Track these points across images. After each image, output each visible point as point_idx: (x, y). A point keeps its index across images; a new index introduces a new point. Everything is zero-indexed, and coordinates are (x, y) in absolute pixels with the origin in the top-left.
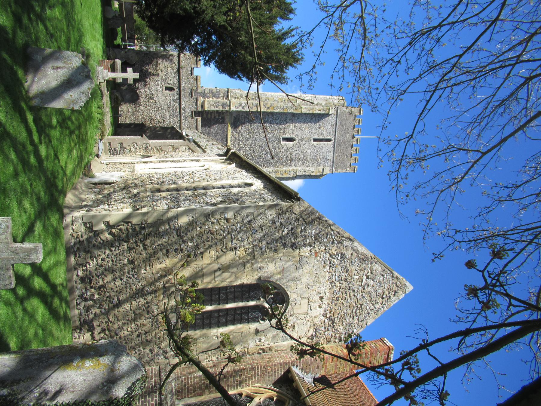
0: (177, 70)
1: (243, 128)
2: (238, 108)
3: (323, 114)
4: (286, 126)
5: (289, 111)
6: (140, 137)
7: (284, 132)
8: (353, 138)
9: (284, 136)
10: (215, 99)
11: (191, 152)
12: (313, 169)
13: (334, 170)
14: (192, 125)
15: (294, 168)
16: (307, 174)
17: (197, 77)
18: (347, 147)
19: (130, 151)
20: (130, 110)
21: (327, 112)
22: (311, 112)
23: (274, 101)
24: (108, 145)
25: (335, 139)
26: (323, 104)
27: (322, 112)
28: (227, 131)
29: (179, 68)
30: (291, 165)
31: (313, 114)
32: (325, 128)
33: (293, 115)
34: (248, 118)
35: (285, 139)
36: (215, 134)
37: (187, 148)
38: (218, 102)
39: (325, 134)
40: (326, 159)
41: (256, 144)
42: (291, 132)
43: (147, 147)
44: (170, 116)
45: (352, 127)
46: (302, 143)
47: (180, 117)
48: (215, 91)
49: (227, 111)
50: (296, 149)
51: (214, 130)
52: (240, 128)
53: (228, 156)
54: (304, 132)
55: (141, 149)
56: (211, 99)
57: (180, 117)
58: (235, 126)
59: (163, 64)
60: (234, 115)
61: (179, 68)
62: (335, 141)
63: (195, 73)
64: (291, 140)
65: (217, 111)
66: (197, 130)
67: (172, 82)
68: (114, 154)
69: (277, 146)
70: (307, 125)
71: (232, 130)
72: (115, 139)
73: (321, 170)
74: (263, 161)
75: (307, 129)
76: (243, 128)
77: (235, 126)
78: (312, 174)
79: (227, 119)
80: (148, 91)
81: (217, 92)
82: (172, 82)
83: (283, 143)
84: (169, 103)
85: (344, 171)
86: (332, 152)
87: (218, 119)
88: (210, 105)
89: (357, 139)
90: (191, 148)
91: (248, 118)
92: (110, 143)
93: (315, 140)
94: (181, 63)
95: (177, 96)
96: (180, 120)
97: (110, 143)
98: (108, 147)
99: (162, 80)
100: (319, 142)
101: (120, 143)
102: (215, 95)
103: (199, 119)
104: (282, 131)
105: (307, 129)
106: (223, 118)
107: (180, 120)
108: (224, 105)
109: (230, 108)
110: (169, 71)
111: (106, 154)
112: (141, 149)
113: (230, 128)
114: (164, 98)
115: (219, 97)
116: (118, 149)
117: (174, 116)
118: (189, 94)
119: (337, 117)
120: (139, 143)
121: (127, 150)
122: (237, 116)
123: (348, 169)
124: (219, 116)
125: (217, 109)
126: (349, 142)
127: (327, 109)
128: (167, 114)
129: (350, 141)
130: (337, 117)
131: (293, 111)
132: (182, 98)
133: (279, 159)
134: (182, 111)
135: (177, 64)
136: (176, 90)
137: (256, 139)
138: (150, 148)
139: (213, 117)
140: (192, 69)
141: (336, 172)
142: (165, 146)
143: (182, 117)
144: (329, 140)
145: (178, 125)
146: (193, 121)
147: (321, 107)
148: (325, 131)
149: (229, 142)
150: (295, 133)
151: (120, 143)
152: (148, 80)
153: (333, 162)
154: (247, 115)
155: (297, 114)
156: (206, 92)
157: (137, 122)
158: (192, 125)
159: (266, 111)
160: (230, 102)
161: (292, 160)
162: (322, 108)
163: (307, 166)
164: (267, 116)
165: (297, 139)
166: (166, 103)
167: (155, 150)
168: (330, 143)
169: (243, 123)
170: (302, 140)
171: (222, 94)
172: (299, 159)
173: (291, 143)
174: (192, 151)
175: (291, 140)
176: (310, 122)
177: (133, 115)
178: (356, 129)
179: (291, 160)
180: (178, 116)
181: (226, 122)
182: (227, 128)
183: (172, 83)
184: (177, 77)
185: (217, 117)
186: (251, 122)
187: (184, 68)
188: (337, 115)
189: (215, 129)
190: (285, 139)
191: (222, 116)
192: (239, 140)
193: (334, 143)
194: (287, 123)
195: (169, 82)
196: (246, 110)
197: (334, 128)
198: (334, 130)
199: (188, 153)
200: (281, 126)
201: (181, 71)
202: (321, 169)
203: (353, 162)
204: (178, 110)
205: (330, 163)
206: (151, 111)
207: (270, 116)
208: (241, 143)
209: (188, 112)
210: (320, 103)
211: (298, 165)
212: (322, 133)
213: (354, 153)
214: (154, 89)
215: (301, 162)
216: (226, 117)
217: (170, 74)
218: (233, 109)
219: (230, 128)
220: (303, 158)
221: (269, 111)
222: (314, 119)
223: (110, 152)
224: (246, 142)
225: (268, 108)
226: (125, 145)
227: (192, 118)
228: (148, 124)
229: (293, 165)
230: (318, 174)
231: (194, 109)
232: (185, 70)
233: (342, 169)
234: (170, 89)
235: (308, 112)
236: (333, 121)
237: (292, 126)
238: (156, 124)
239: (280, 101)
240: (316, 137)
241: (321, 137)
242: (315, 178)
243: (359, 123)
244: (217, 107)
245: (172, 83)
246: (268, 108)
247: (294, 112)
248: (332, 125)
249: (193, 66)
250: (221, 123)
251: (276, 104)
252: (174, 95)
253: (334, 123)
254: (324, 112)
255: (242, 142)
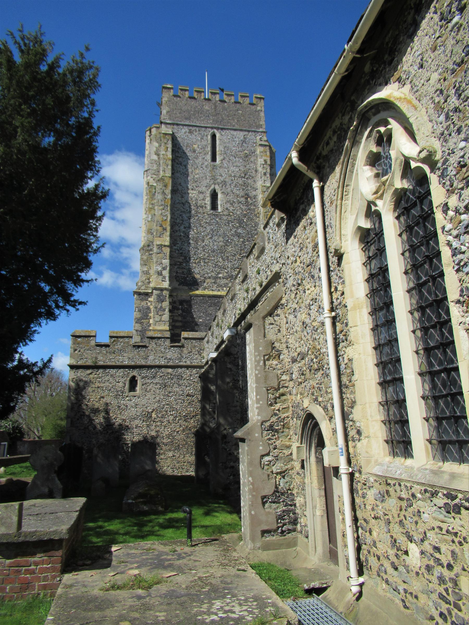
0: (101, 371)
1: (196, 271)
2: (164, 277)
3: (173, 142)
4: (193, 203)
5: (169, 196)
6: (243, 449)
7: (202, 207)
8: (209, 100)
9: (209, 207)
10: (151, 315)
11: (279, 311)
12: (260, 161)
13: (261, 130)
14: (195, 347)
15: (259, 191)
16: (268, 170)
17: (111, 337)
18: (224, 109)
19: (283, 474)
20: (171, 454)
21: (170, 138)
22: (170, 163)
23: (152, 220)
24: (268, 538)
25: (212, 128)
26: (156, 145)
27: (170, 145)
28: (202, 296)
29: (96, 367)
30: (255, 197)
31: (173, 160)
32: (195, 143)
33: (174, 191)
34: (181, 263)
35: (214, 206)
36: (206, 316)
37: (269, 320)
38: (156, 308)
39: (204, 143)
40: (244, 141)
41: (222, 251)
42: (201, 196)
43: (271, 428)
44: (179, 385)
45: (193, 102)
46: (220, 179)
47: (181, 367)
48: (137, 314)
49: (170, 296)
50: (229, 189)
51: (200, 317)
52: (197, 276)
53: (310, 174)
54: (202, 175)
55: (278, 443)
56: (151, 321)
57: (181, 367)
58: (194, 284)
59: (93, 399)
60: (176, 284)
61: (96, 367)
62: (215, 128)
63: (106, 340)
64: (214, 196)
65: (170, 311)
66: (203, 339)
67: (120, 379)
68: (295, 522)
69: (225, 218)
70: (190, 170)
71: (201, 289)
72: (253, 518)
73: (262, 149)
74: (248, 241)
75: (197, 171)
76: (198, 271)
77: (194, 284)
78: (269, 162)
79: (183, 296)
80: (137, 422)
81: (140, 311)
82: (120, 379)
83: (220, 209)
84: (158, 386)
85: (262, 114)
86: (232, 132)
87: (183, 311)
88: (160, 324)
89: (212, 93)
90: (268, 308)
91: (181, 263)
92: (264, 532)
93: (214, 159)
94: (87, 364)
95: (144, 372)
96: (187, 367)
97: (264, 532)
98: (275, 538)
99: (116, 397)
100: (218, 153)
101: (264, 504)
102: (144, 314)
103: (185, 334)
104: (200, 210)
105: (197, 171)
106: (181, 302)
107: (187, 367)
108: (160, 299)
109: (166, 289)
110: (102, 385)
111: (295, 544)
112: (278, 443)
113: (197, 292)
114: (149, 395)
115: (148, 308)
116: (282, 508)
117: (180, 377)
118: (142, 352)
119: (177, 125)
120: (261, 449)
121: (282, 484)
122: (177, 281)
123: (259, 108)
124: (178, 309)
125: (167, 310)
126: (216, 107)
127: (164, 138)
128: (176, 389)
129: (215, 104)
130: (177, 125)
131: (168, 191)
132: (149, 363)
133: (245, 216)
134: (171, 363)
135: (89, 371)
136: (135, 373)
137: (214, 251)
138: (274, 419)
139: (180, 319)
140: (97, 345)
141: (264, 127)
142: (266, 378)
143: (181, 364)
144: (214, 136)
145: (194, 371)
146: (189, 345)
147: (163, 147)
148: (199, 143)
149: (219, 293)
150: (204, 189)
151: (264, 504)
152: (118, 422)
153: (249, 131)
154: (175, 265)
155: (173, 187)
156: (140, 328)
157: (192, 440)
158: (195, 347)
159: (168, 233)
160: (155, 289)
161: (246, 194)
162: (163, 144)
163: (256, 171)
164: (177, 234)
165: (212, 187)
166: (158, 391)
167: (277, 406)
168: (218, 135)
169: (190, 272)
170: (214, 178)
171: (144, 303)
172: (245, 185)
173: (220, 196)
174: (276, 307)
175: (214, 196)
176: (186, 166)
177: (178, 448)
178: (195, 95)
179: (247, 196)
180: (180, 370)
181: (188, 298)
182: (197, 296)
183: (123, 380)
184: (113, 371)
185: (180, 312)
186: (187, 259)
187: (96, 358)
188: (173, 124)
189: (199, 315)
190: (214, 206)
191: (178, 303)
192: (216, 278)
193: (218, 129)
194: (187, 202)
195: (121, 384)
196: (168, 264)
197: (194, 128)
198: (197, 129)
199: (282, 317)
200: (193, 212)
201: (101, 363)
202: (259, 150)
203: (247, 101)
204: (170, 370)
205: (251, 136)
206: (171, 418)
207: (177, 228)
208: (220, 275)
209: (172, 354)
210: (155, 149)
211: (255, 186)
212: (204, 148)
213: (233, 99)
214: (133, 412)
215: (249, 181)
216: (180, 298)
217: (107, 384)
218: (166, 284)
219: (197, 292)
220: (242, 177)
221: (169, 228)
222: (180, 159)
223: (290, 531)
224: (220, 267)
225: (165, 229)
226: (268, 490)
227: (183, 346)
228: (194, 423)
229: (254, 193)
230: (268, 153)
231: (168, 342)
232: (100, 358)
233: (259, 118)
234: (133, 383)
235: (170, 167)
236: (183, 131)
237: (192, 194)
238: (196, 408)
239: (152, 212)
240: (209, 157)
241: (209, 149)
242: (275, 160)
243: (186, 90)
244: (164, 310)
245: (123, 380)
246: (165, 229)
247: (170, 188)
248: (190, 132)
249: (93, 343)
250: (190, 306)
251: (158, 218)
252: (143, 378)
253: (186, 129)
254: (170, 142)
255: (219, 273)
